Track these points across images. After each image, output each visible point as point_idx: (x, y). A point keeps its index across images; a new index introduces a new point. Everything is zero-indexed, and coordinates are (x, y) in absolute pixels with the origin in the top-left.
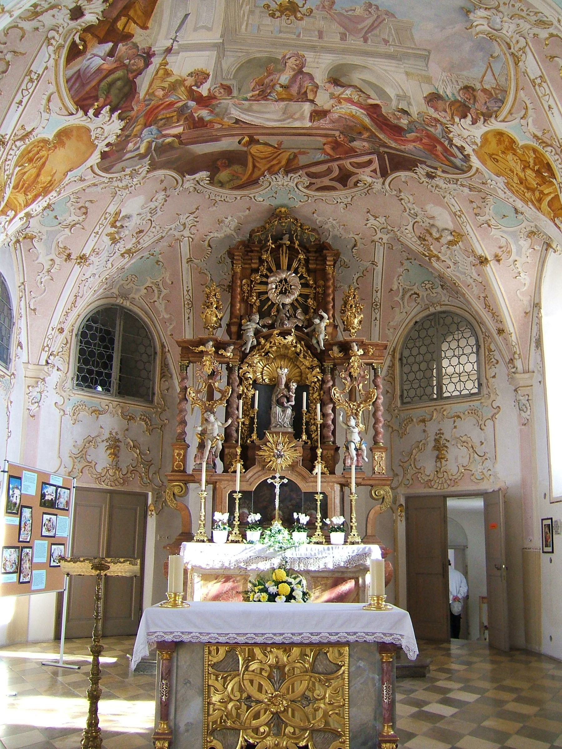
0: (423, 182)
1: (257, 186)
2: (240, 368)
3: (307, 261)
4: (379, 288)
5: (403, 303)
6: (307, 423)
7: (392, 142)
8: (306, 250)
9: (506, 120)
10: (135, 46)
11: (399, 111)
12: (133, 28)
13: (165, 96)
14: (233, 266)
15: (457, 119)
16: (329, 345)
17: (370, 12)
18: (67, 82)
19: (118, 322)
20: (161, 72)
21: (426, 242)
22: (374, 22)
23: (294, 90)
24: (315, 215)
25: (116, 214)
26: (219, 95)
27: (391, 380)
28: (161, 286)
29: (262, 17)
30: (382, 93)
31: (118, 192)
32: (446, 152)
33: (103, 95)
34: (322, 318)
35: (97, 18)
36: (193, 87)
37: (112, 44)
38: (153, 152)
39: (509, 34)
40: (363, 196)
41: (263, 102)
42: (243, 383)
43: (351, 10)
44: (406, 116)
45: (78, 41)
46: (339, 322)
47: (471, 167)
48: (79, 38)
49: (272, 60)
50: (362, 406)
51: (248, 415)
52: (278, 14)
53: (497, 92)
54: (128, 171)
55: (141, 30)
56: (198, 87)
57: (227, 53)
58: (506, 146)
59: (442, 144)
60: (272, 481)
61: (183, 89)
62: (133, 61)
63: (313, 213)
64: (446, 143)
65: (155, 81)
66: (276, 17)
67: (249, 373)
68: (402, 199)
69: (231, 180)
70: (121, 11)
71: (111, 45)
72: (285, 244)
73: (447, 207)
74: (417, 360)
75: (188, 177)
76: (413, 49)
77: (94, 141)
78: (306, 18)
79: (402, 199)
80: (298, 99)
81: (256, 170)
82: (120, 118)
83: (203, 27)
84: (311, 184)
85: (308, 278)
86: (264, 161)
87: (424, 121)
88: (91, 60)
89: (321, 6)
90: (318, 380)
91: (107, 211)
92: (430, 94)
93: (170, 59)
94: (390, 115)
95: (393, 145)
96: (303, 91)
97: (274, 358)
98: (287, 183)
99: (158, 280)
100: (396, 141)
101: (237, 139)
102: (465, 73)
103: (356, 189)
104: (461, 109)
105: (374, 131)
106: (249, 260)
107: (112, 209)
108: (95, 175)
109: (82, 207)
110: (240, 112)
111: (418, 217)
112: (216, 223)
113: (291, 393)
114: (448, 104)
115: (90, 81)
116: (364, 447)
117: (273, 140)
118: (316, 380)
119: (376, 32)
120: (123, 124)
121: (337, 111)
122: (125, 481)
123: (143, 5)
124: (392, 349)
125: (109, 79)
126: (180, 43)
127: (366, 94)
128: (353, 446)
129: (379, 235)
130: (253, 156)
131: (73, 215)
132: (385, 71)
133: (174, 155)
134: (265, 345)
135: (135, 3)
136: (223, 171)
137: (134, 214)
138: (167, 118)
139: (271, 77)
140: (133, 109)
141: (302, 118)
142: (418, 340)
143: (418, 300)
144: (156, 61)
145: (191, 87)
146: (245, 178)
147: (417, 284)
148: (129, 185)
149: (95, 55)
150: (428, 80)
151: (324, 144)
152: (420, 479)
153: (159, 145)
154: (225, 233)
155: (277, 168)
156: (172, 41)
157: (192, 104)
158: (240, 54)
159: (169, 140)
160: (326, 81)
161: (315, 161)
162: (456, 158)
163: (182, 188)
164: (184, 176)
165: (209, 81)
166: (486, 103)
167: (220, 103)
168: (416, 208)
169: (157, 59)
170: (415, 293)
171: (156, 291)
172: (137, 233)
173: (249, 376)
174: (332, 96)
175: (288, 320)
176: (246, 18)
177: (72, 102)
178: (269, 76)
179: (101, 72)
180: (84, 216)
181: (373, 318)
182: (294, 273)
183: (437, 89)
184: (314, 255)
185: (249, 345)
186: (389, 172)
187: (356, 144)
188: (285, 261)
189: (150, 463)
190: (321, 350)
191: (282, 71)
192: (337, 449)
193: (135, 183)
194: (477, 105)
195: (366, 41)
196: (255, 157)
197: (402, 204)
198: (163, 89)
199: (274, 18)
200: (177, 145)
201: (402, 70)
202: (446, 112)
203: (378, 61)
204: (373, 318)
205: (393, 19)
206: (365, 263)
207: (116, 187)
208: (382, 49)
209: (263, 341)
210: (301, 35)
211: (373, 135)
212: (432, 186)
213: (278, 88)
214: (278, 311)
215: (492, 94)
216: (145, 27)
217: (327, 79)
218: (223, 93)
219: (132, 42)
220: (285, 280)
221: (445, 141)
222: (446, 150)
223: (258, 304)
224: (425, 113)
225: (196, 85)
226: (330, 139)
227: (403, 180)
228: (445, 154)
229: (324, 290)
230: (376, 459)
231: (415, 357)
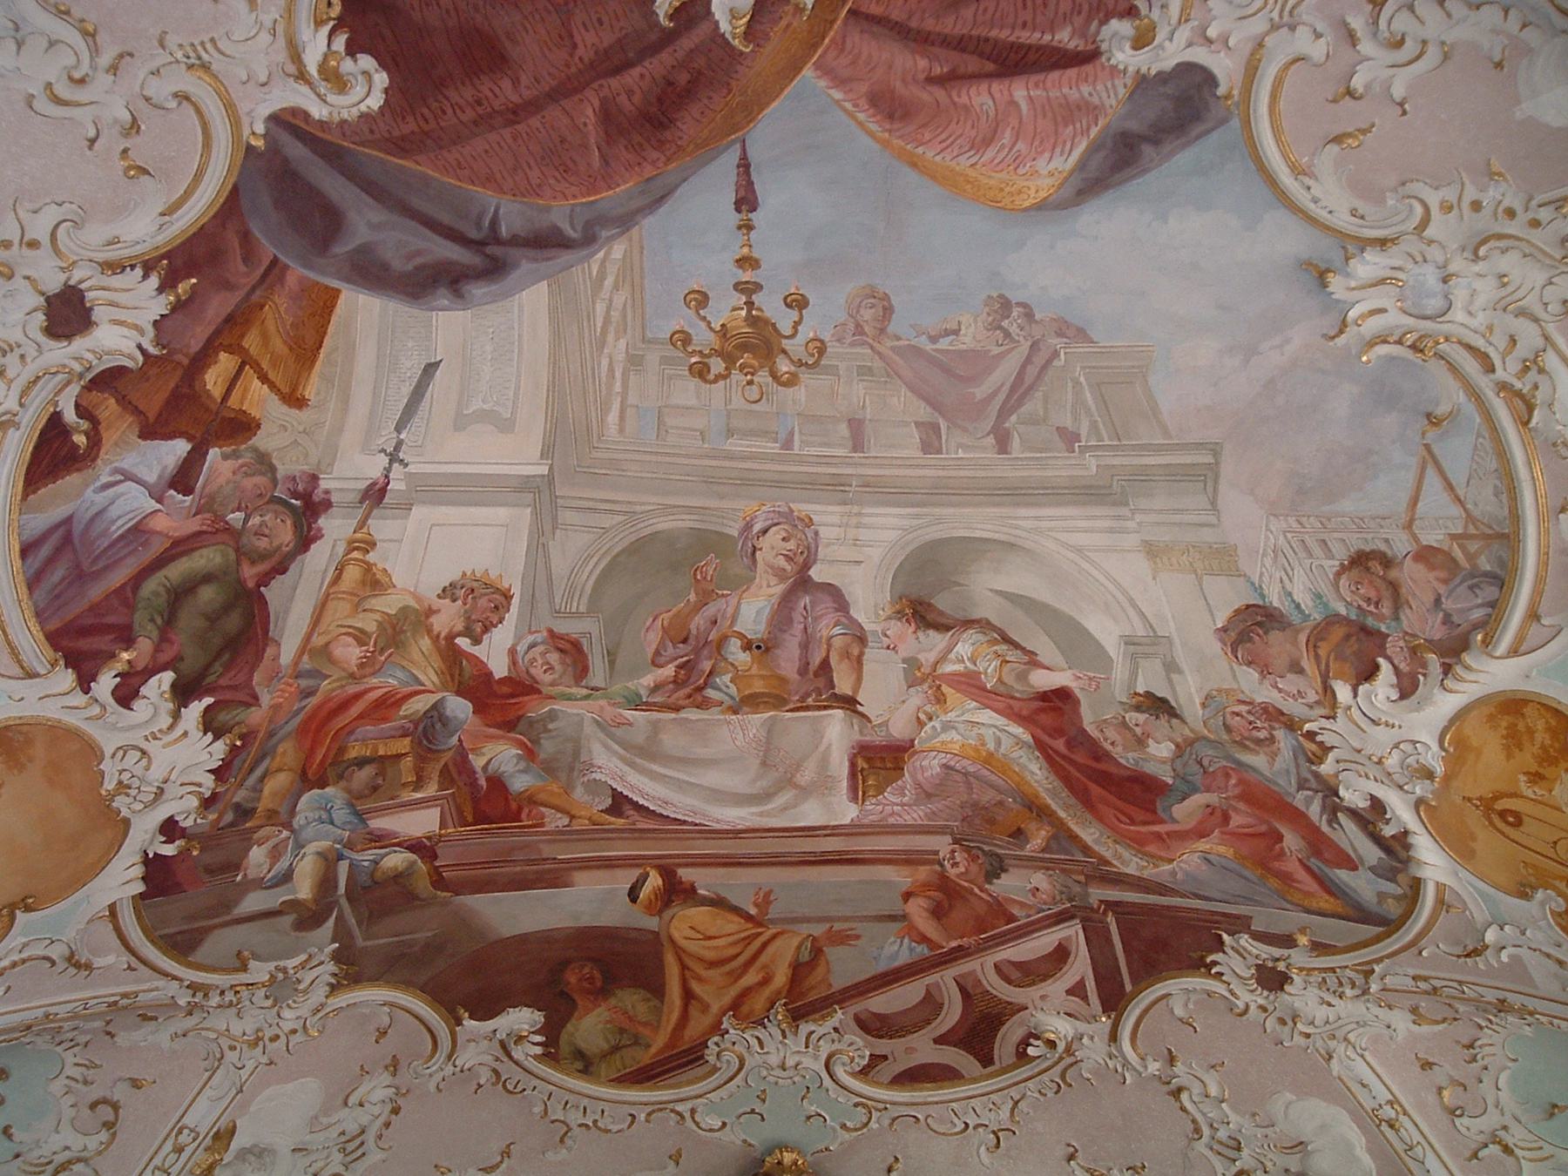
0: (1247, 1006)
1: (699, 1071)
7: (1126, 854)
9: (1523, 649)
10: (264, 462)
11: (1138, 708)
12: (257, 398)
13: (368, 665)
15: (1343, 692)
17: (1007, 335)
18: (25, 552)
20: (352, 573)
22: (1024, 367)
23: (788, 660)
25: (217, 1136)
26: (547, 678)
29: (670, 378)
30: (1076, 641)
31: (228, 1054)
32: (1317, 853)
33: (150, 626)
35: (140, 347)
36: (459, 641)
37: (188, 447)
38: (344, 902)
39: (1480, 320)
40: (1050, 1094)
41: (692, 714)
43: (947, 333)
44: (1164, 719)
45: (70, 416)
47: (1417, 885)
48: (77, 406)
49: (707, 542)
52: (717, 365)
53: (1473, 547)
54: (260, 971)
55: (285, 408)
56: (477, 641)
57: (567, 516)
58: (1543, 747)
59: (1297, 817)
61: (426, 643)
62: (255, 520)
64: (1314, 811)
65: (331, 605)
66: (711, 377)
68: (1180, 1090)
69: (616, 1049)
70: (217, 332)
71: (181, 447)
73: (1341, 1093)
75: (469, 1023)
76: (1159, 449)
77: (112, 796)
78: (804, 376)
79: (1180, 1090)
80: (803, 699)
81: (694, 1012)
82: (210, 724)
83: (484, 416)
84: (877, 1059)
86: (713, 974)
87: (1228, 729)
88: (111, 491)
89: (852, 326)
91: (186, 1121)
92: (1237, 612)
93: (382, 527)
94: (1111, 734)
95: (1132, 864)
96: (816, 660)
98: (797, 1058)
100: (1138, 844)
101: (626, 878)
102: (1347, 505)
103: (1024, 1072)
104: (1353, 645)
105: (1062, 814)
107: (203, 1116)
108: (134, 962)
109: (105, 1101)
110: (622, 759)
111: (1245, 1153)
114: (1303, 638)
115: (107, 568)
117: (740, 886)
119: (1033, 406)
120: (220, 748)
121: (936, 742)
123: (289, 320)
125: (176, 571)
126: (411, 469)
127: (1023, 649)
130: (679, 952)
131: (66, 1127)
132: (1079, 550)
133: (419, 927)
135: (262, 307)
136: (588, 1011)
137: (284, 1144)
138: (382, 761)
139: (710, 610)
140: (256, 698)
141: (823, 785)
144: (335, 528)
145: (451, 638)
146: (660, 1040)
148: (268, 1034)
149: (129, 477)
150: (1223, 559)
151: (907, 896)
153: (364, 879)
155: (758, 1003)
156: (384, 460)
157: (459, 708)
158: (608, 521)
159: (396, 860)
160: (889, 612)
161: (882, 967)
162: (1354, 868)
164: (459, 1022)
165: (512, 617)
166: (1438, 601)
167: (552, 716)
168: (1233, 1117)
169: (338, 522)
174: (915, 675)
176: (618, 387)
177: (35, 628)
178: (702, 605)
179: (145, 544)
180: (104, 1136)
183: (1263, 596)
186: (1128, 987)
187: (1011, 885)
191: (743, 583)
193: (287, 1026)
194: (1409, 619)
195: (1003, 445)
196: (687, 961)
197: (1183, 1109)
198: (361, 637)
199: (706, 381)
200: (423, 885)
201: (1132, 540)
202: (1301, 671)
203: (1052, 519)
205: (1082, 348)
207: (220, 1034)
208: (1062, 468)
210: (797, 444)
211: (1063, 837)
212: (1282, 1022)
213: (736, 653)
215: (1454, 560)
216: (295, 400)
217: (892, 603)
218: (558, 667)
219: (256, 450)
221: (1309, 801)
222: (1318, 843)
224: (1227, 692)
225: (467, 632)
226: (923, 873)
227: (1179, 1012)
228: (1314, 863)
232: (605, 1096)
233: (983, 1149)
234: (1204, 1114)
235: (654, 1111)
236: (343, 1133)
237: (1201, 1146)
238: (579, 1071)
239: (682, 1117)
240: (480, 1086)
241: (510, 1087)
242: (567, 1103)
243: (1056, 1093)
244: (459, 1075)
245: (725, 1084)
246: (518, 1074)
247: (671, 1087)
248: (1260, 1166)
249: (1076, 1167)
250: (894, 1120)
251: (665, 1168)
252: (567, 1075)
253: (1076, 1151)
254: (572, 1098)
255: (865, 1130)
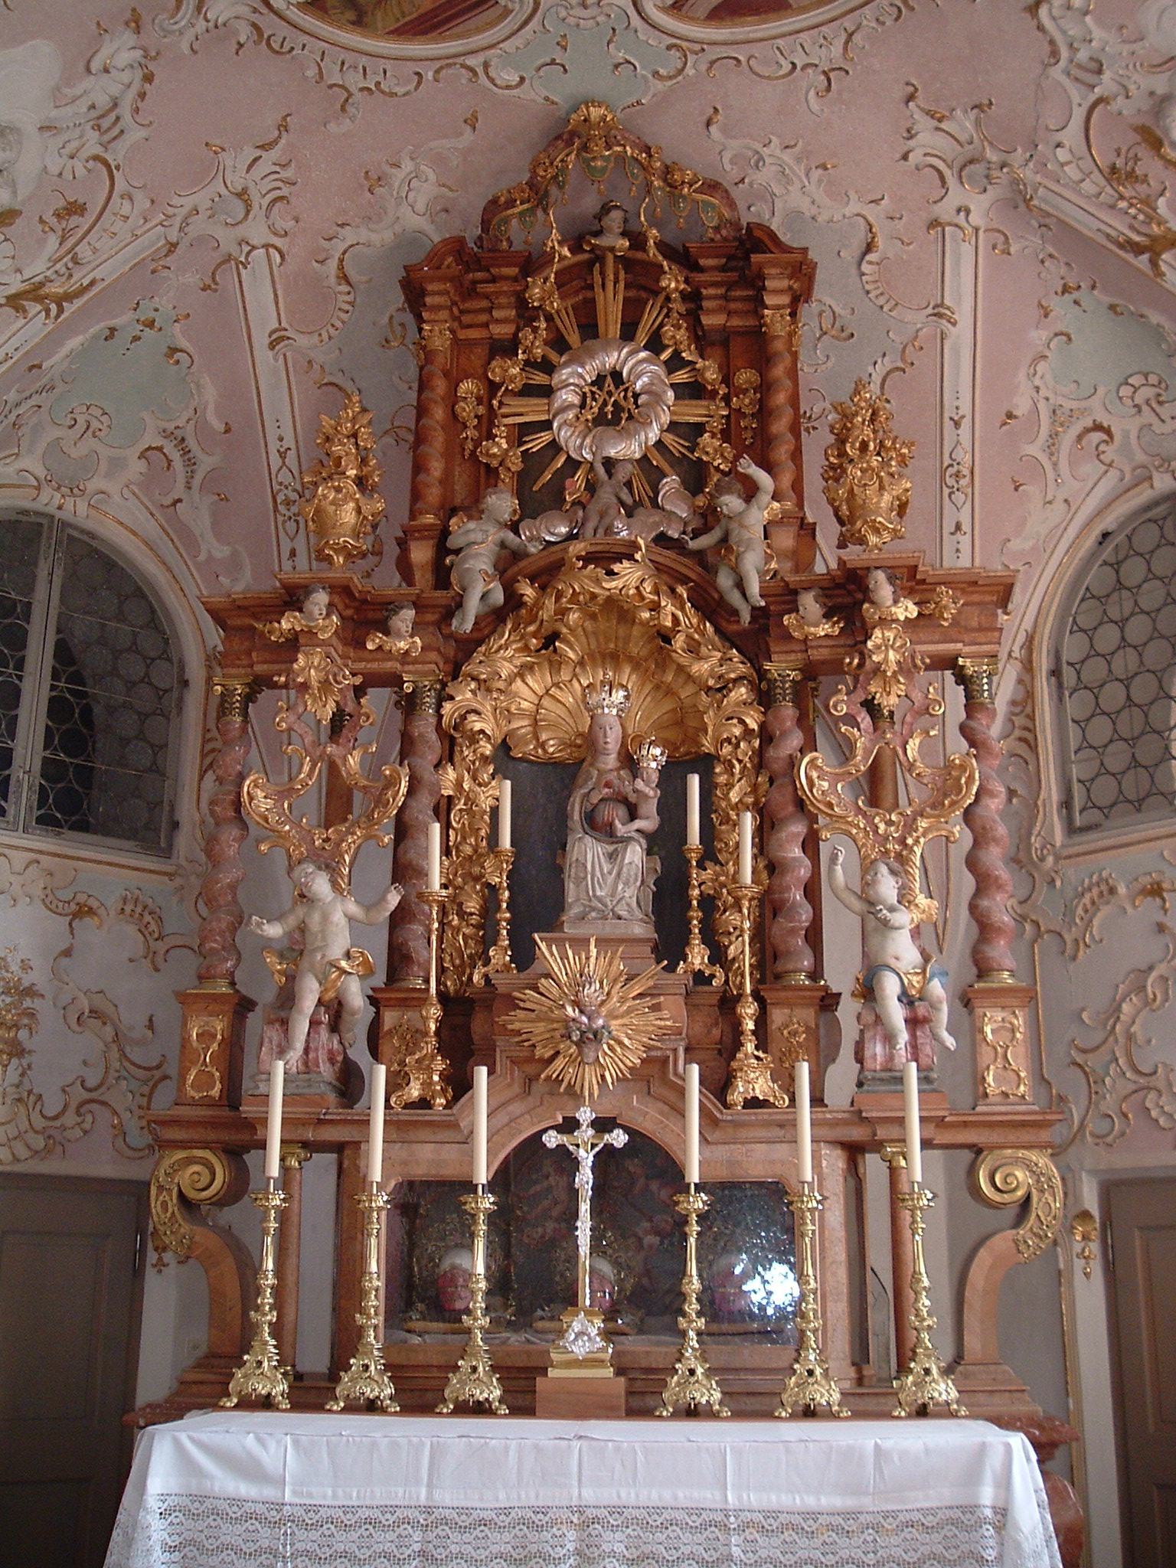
2: (443, 697)
3: (693, 297)
4: (966, 409)
5: (1055, 464)
6: (708, 903)
8: (683, 258)
14: (420, 330)
16: (785, 596)
19: (42, 573)
21: (1142, 189)
24: (713, 129)
27: (1022, 749)
28: (191, 443)
34: (750, 491)
42: (457, 758)
46: (817, 511)
50: (923, 823)
51: (477, 879)
60: (564, 1139)
63: (708, 124)
67: (478, 713)
72: (612, 249)
74: (1145, 603)
85: (700, 364)
90: (748, 732)
97: (581, 663)
99: (181, 423)
106: (482, 310)
111: (1106, 76)
112: (361, 186)
113: (640, 784)
116: (937, 988)
118: (737, 731)
122: (54, 1144)
124: (1021, 638)
128: (890, 986)
129: (957, 194)
134: (538, 605)
142: (1115, 596)
143: (1110, 452)
147: (1101, 391)
152: (1154, 1114)
154: (398, 228)
163: (201, 25)
168: (1097, 33)
170: (1098, 427)
171: (176, 456)
172: (58, 215)
173: (478, 726)
175: (630, 515)
181: (949, 526)
182: (645, 348)
184: (718, 277)
185: (473, 606)
188: (611, 307)
189: (157, 1074)
190: (754, 608)
192: (828, 1002)
197: (1040, 28)
204: (949, 526)
206: (909, 316)
209: (528, 591)
214: (591, 487)
220: (616, 375)
223: (515, 463)
229: (761, 400)
230: (990, 1037)
231: (1108, 658)
232: (385, 52)
233: (812, 93)
234: (1064, 32)
235: (442, 68)
236: (93, 107)
237: (1057, 73)
238: (353, 23)
239: (475, 73)
240: (241, 45)
241: (276, 46)
242: (343, 63)
243: (897, 19)
244: (214, 31)
245: (519, 30)
246: (283, 30)
247: (459, 37)
248: (1122, 91)
249: (916, 109)
250: (712, 63)
251: (462, 134)
252: (340, 28)
253: (916, 90)
254: (349, 58)
255: (680, 78)
